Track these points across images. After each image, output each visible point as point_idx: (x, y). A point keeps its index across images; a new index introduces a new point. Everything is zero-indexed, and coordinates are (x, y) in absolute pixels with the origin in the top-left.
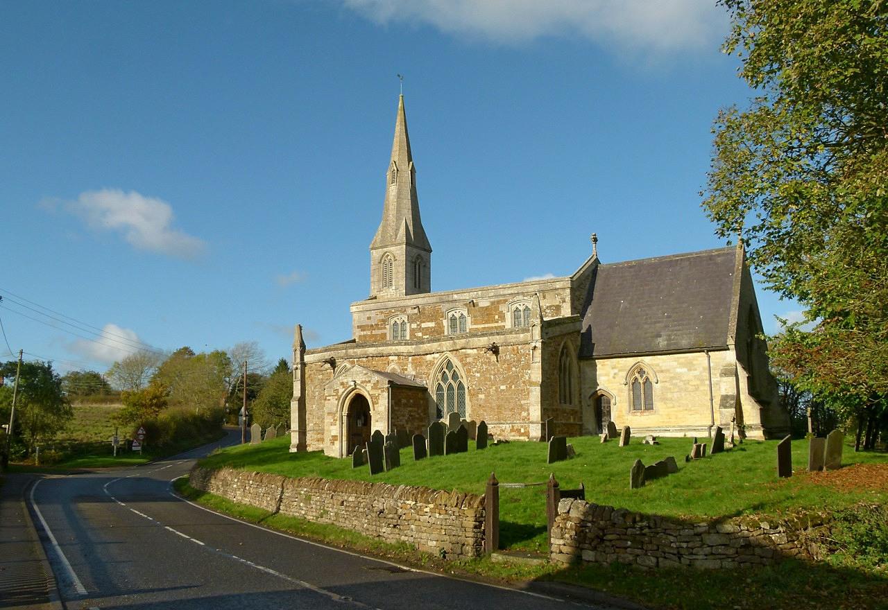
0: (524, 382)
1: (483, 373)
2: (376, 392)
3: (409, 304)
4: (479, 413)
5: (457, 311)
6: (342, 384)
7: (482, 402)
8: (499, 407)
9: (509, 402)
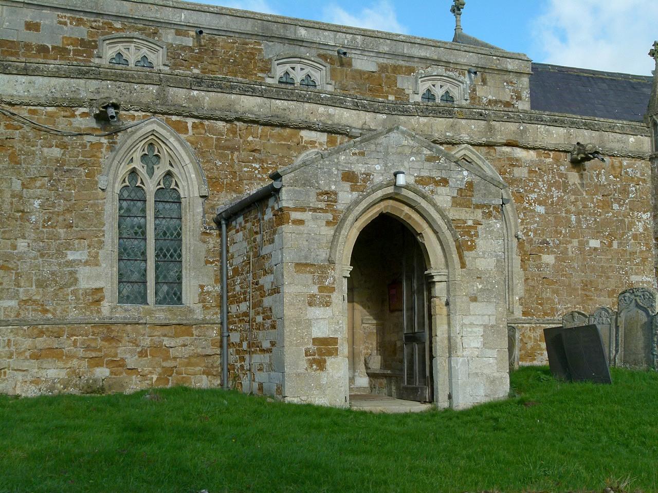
0: (635, 237)
1: (552, 208)
2: (469, 216)
3: (176, 20)
4: (544, 295)
5: (298, 67)
6: (349, 177)
7: (548, 272)
8: (586, 285)
9: (608, 277)
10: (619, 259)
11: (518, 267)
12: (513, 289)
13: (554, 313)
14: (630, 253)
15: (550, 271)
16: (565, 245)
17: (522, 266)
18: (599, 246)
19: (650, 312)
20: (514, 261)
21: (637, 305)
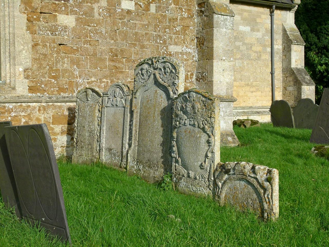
4: (59, 66)
7: (65, 38)
9: (143, 47)
10: (156, 26)
11: (22, 29)
12: (14, 58)
13: (73, 89)
14: (170, 20)
15: (68, 36)
16: (89, 4)
17: (28, 28)
18: (134, 9)
19: (171, 93)
20: (16, 20)
21: (157, 83)
